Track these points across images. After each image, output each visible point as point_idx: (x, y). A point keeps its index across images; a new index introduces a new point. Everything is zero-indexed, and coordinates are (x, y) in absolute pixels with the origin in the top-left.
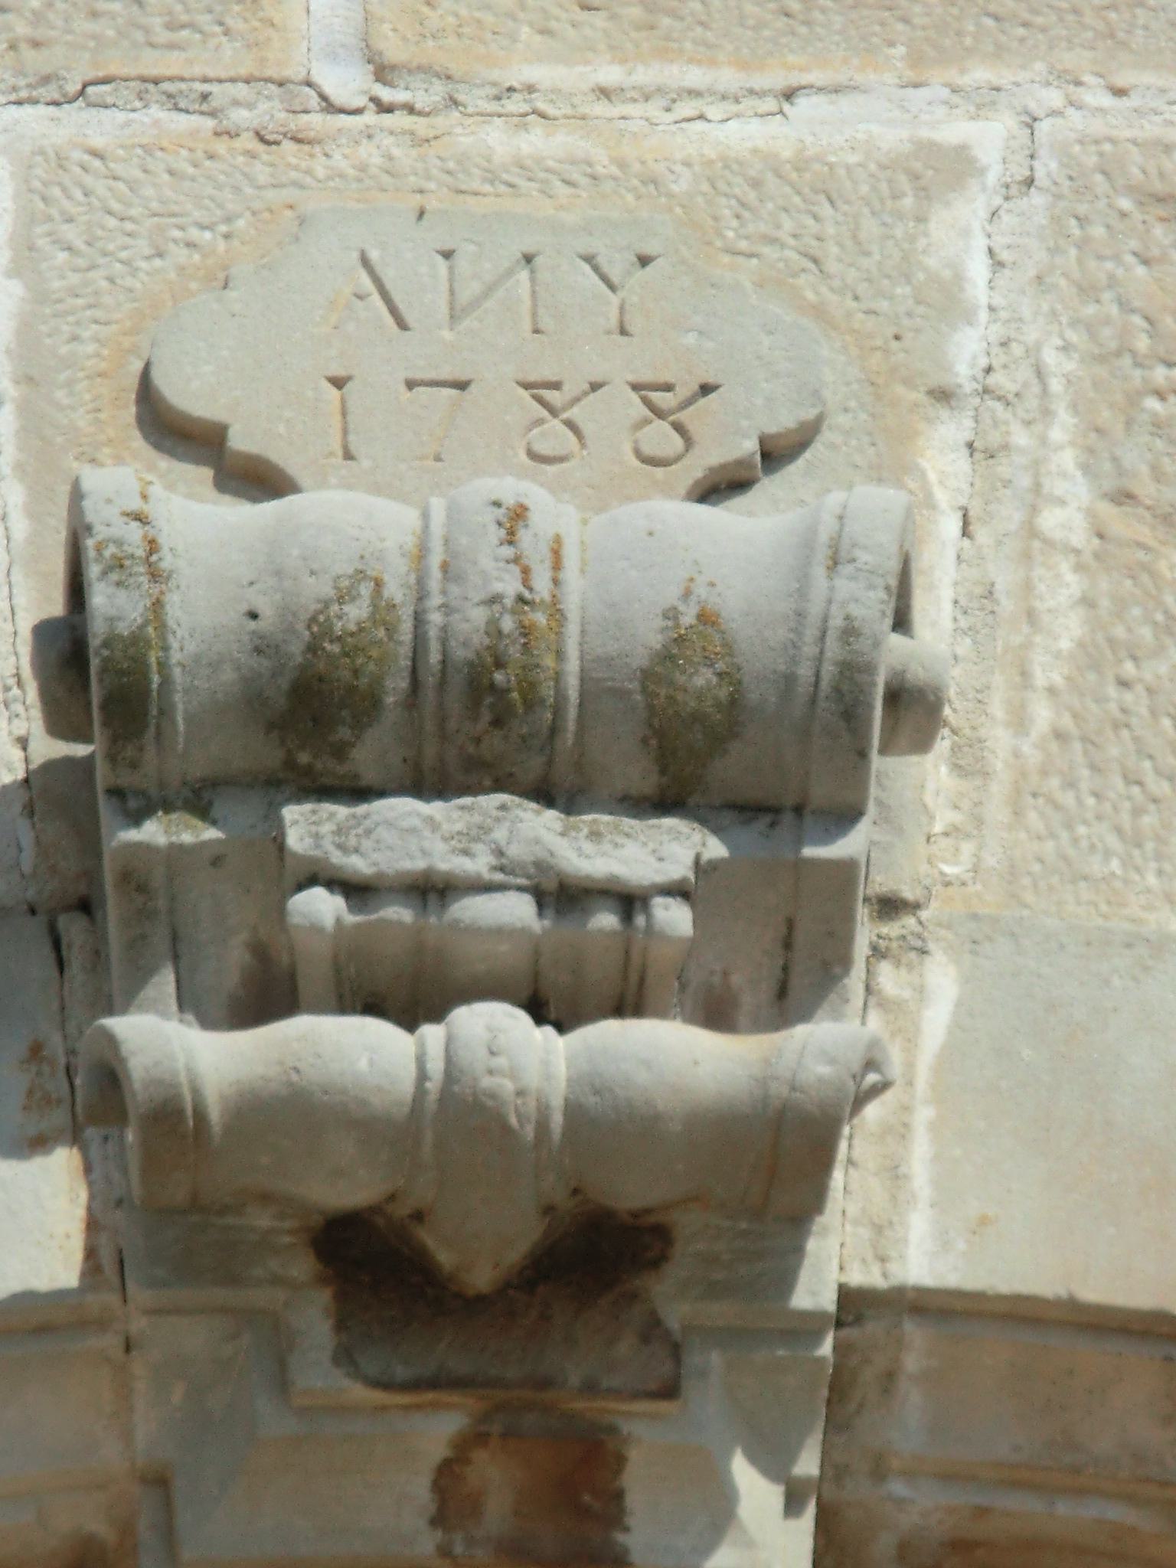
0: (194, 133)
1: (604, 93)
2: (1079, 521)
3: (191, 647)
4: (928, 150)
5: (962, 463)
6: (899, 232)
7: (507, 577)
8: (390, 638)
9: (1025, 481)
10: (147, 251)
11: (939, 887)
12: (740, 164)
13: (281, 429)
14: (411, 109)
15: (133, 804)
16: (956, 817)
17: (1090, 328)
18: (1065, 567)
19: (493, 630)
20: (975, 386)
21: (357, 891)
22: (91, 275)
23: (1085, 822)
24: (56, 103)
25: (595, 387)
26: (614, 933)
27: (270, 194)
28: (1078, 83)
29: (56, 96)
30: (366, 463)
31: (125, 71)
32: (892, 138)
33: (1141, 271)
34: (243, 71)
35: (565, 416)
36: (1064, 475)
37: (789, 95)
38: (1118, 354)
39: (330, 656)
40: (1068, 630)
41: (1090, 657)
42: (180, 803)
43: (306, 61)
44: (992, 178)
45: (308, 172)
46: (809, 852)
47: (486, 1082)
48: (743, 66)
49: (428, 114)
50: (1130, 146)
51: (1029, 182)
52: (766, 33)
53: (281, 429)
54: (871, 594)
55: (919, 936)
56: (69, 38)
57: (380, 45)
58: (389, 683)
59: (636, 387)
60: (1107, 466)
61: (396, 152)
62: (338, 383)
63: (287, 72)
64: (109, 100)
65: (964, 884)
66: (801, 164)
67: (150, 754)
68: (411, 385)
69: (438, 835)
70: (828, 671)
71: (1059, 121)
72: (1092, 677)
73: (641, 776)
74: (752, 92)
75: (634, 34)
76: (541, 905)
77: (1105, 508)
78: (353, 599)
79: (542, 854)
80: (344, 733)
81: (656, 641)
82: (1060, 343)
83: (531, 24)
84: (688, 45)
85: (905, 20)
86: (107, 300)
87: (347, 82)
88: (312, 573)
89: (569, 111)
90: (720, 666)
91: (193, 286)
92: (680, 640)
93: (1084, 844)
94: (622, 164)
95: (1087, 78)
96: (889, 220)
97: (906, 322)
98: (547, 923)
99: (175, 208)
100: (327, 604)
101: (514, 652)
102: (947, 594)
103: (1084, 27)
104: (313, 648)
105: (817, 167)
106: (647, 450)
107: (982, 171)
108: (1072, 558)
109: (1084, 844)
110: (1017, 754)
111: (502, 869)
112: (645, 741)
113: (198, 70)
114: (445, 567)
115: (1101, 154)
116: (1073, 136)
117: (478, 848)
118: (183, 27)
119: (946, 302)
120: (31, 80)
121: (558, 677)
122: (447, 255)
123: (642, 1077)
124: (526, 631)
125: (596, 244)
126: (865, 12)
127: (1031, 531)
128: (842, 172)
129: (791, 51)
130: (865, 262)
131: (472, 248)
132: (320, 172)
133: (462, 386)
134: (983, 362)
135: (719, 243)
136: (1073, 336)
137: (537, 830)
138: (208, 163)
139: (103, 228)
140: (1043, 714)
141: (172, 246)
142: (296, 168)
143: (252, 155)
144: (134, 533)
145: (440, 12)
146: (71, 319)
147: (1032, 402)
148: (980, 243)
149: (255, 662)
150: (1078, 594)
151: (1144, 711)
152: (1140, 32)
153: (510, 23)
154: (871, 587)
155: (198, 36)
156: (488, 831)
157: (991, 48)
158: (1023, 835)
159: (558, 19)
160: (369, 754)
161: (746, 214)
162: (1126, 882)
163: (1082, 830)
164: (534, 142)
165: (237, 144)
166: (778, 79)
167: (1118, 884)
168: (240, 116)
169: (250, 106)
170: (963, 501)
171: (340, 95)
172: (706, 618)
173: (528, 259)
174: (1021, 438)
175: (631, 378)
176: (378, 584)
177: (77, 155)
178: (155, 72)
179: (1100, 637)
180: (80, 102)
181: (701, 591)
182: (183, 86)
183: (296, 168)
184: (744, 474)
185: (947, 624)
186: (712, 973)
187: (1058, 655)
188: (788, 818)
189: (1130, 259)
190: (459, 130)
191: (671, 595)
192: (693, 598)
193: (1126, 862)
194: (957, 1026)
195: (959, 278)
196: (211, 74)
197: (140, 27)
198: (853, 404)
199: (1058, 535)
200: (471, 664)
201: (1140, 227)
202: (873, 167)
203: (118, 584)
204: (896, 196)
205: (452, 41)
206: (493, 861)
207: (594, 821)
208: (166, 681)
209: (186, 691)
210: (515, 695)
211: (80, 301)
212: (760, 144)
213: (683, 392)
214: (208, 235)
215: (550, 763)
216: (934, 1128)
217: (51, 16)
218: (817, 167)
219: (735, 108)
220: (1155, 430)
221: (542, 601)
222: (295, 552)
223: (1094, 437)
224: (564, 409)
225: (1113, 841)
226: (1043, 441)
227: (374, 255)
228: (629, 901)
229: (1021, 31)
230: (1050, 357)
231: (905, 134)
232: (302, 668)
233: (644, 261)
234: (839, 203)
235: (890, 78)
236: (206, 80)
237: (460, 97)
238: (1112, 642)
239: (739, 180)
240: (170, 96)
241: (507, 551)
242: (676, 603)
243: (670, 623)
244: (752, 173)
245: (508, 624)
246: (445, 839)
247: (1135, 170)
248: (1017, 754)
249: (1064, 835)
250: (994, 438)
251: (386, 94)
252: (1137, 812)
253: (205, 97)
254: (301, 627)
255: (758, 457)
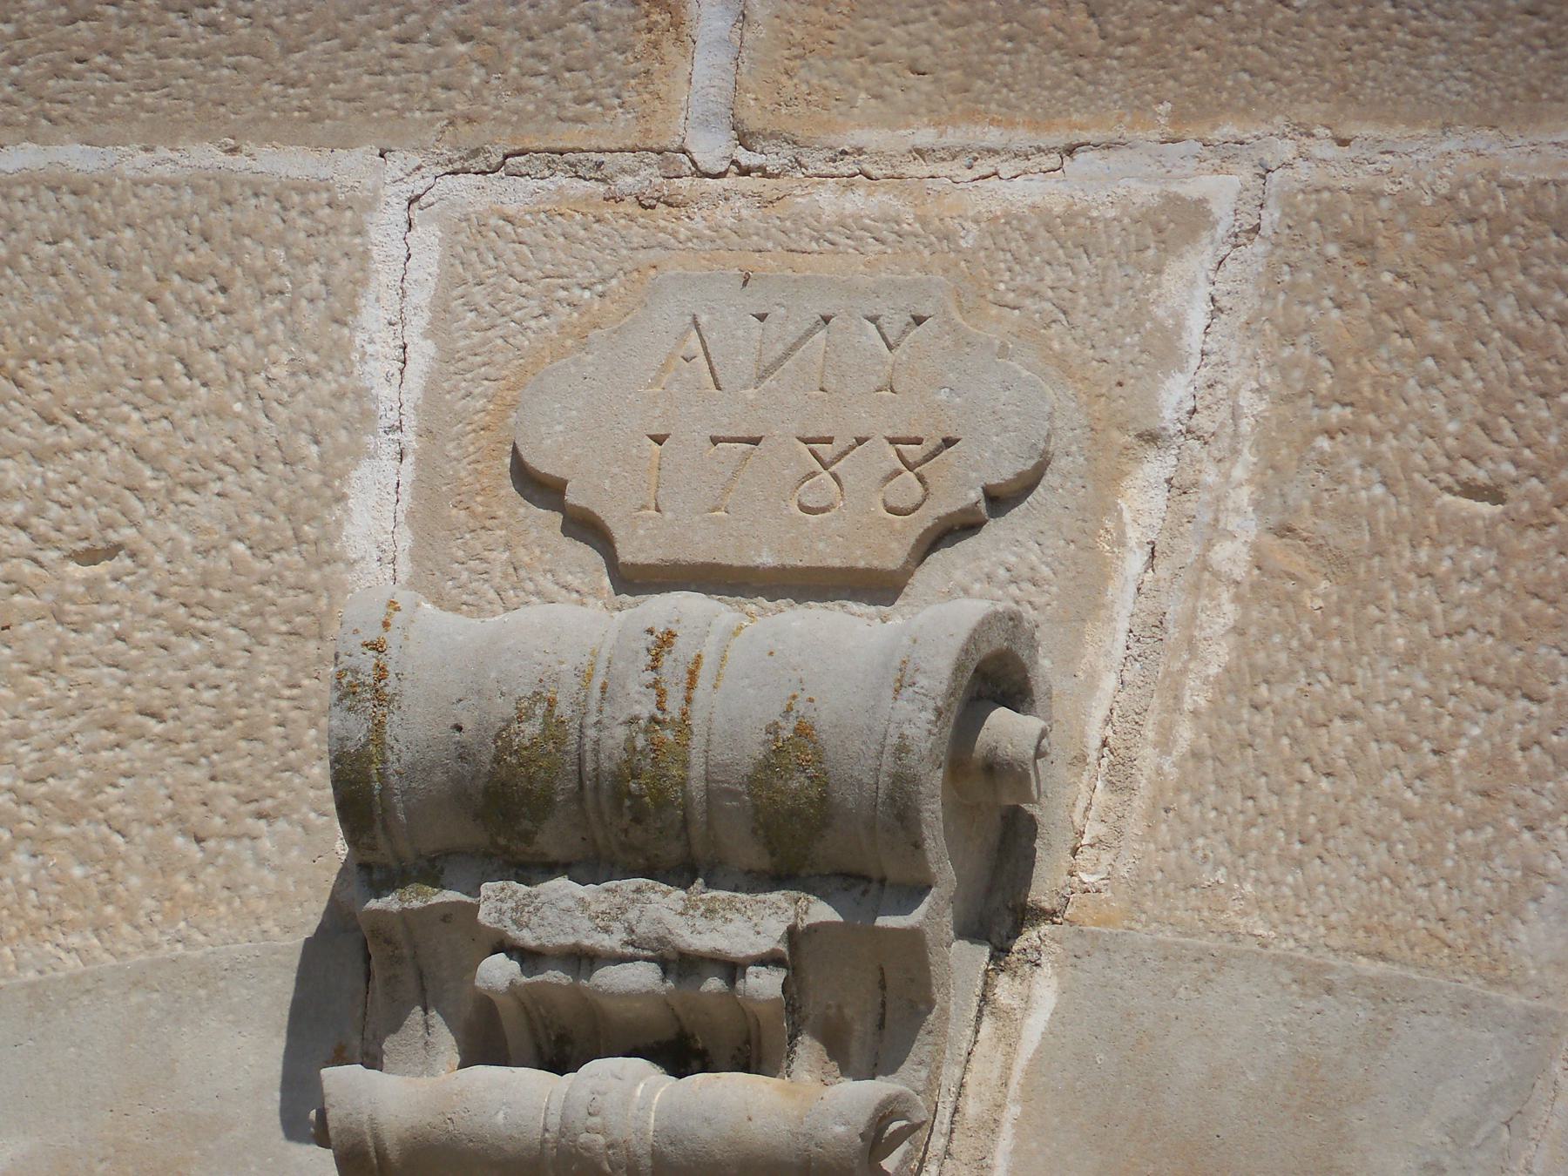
0: (587, 199)
1: (920, 153)
2: (1244, 555)
3: (407, 757)
4: (1173, 202)
5: (1160, 498)
6: (1137, 284)
7: (644, 699)
8: (558, 750)
9: (1207, 517)
10: (537, 312)
11: (1078, 894)
12: (1019, 219)
13: (607, 484)
14: (762, 170)
15: (376, 876)
16: (1101, 830)
17: (1284, 369)
18: (1225, 596)
19: (630, 748)
20: (1180, 427)
21: (530, 958)
22: (489, 333)
23: (1203, 835)
24: (484, 173)
25: (860, 441)
26: (720, 994)
27: (641, 255)
28: (1310, 135)
29: (484, 168)
30: (669, 515)
31: (536, 145)
32: (1145, 193)
33: (1335, 314)
34: (629, 143)
35: (833, 468)
36: (1237, 511)
37: (1070, 151)
38: (1302, 395)
39: (510, 766)
40: (1218, 656)
41: (1232, 683)
42: (415, 873)
43: (682, 132)
44: (1221, 231)
45: (674, 234)
46: (881, 921)
47: (583, 1138)
48: (1034, 125)
49: (777, 176)
50: (1344, 193)
51: (1256, 229)
52: (1060, 92)
53: (607, 484)
54: (923, 715)
55: (1038, 950)
56: (499, 113)
57: (743, 114)
58: (558, 786)
59: (893, 441)
60: (1277, 501)
61: (745, 213)
62: (659, 440)
63: (665, 143)
64: (524, 170)
65: (1098, 891)
66: (1069, 219)
67: (381, 839)
68: (715, 441)
69: (586, 915)
70: (884, 780)
71: (1289, 172)
72: (1231, 699)
73: (753, 856)
74: (1039, 150)
75: (951, 97)
76: (665, 972)
77: (1269, 539)
78: (529, 718)
79: (662, 932)
80: (526, 824)
81: (759, 752)
82: (1255, 385)
83: (867, 90)
84: (993, 106)
85: (1175, 78)
86: (499, 358)
87: (712, 148)
88: (502, 694)
89: (889, 172)
90: (811, 771)
91: (569, 342)
92: (778, 752)
93: (1200, 854)
94: (923, 220)
95: (1319, 131)
96: (1131, 272)
97: (1130, 369)
98: (670, 984)
99: (565, 270)
100: (509, 722)
101: (646, 764)
102: (1123, 625)
103: (1324, 80)
104: (497, 760)
105: (1081, 221)
106: (892, 502)
107: (1214, 225)
108: (1233, 590)
109: (1200, 854)
110: (1159, 771)
111: (632, 944)
112: (754, 831)
113: (594, 143)
114: (604, 689)
115: (1319, 202)
116: (1298, 186)
117: (616, 926)
118: (589, 101)
119: (1164, 350)
120: (464, 154)
121: (684, 782)
122: (762, 318)
123: (705, 1133)
124: (656, 747)
125: (880, 306)
126: (1144, 71)
127: (1204, 565)
128: (1100, 226)
129: (1077, 111)
130: (1107, 313)
131: (783, 311)
132: (683, 234)
133: (755, 441)
134: (1189, 405)
135: (990, 296)
136: (1268, 379)
137: (664, 909)
138: (596, 226)
139: (504, 290)
140: (1185, 733)
141: (557, 305)
142: (663, 230)
143: (631, 218)
144: (368, 661)
145: (796, 80)
146: (469, 376)
147: (1225, 442)
148: (1204, 290)
149: (455, 766)
150: (1231, 623)
151: (1268, 731)
152: (1370, 84)
153: (851, 89)
154: (924, 709)
155: (599, 109)
156: (622, 910)
157: (1242, 103)
158: (1152, 846)
159: (890, 85)
160: (550, 840)
161: (1017, 268)
162: (1230, 890)
163: (1200, 842)
164: (859, 202)
165: (621, 208)
166: (1061, 138)
167: (1221, 891)
168: (625, 182)
169: (633, 173)
170: (1153, 537)
171: (708, 162)
172: (803, 731)
173: (826, 320)
174: (1210, 476)
175: (889, 433)
176: (552, 703)
177: (494, 221)
178: (560, 145)
179: (1244, 663)
180: (501, 173)
181: (800, 706)
182: (581, 156)
183: (663, 230)
184: (971, 519)
185: (1119, 653)
186: (829, 1007)
187: (1206, 681)
188: (874, 887)
189: (1327, 303)
190: (798, 191)
191: (774, 713)
192: (793, 713)
193: (1233, 872)
194: (1050, 1032)
195: (1180, 326)
196: (604, 146)
197: (554, 102)
198: (1074, 448)
199: (1225, 567)
200: (612, 773)
201: (1342, 272)
202: (1126, 220)
203: (349, 709)
204: (1141, 250)
205: (801, 108)
206: (625, 936)
207: (713, 899)
208: (386, 788)
209: (404, 793)
210: (647, 799)
211: (478, 359)
212: (1038, 199)
213: (928, 446)
214: (587, 294)
215: (688, 844)
216: (1017, 1124)
217: (485, 93)
218: (1081, 221)
219: (1024, 164)
220: (1319, 467)
221: (672, 720)
222: (493, 675)
223: (1271, 474)
224: (833, 463)
225: (1223, 851)
226: (1227, 476)
227: (703, 319)
228: (732, 969)
229: (1270, 85)
230: (1246, 399)
231: (1157, 189)
232: (491, 774)
233: (919, 320)
234: (1093, 256)
235: (1154, 135)
236: (600, 151)
237: (804, 160)
238: (1252, 666)
239: (1017, 235)
240: (572, 165)
241: (650, 677)
242: (779, 719)
243: (771, 737)
244: (1028, 228)
245: (640, 742)
246: (591, 918)
247: (1345, 217)
248: (1159, 771)
249: (1186, 845)
250: (1189, 476)
251: (746, 158)
252: (1249, 825)
253: (599, 165)
254: (489, 741)
255: (983, 506)
